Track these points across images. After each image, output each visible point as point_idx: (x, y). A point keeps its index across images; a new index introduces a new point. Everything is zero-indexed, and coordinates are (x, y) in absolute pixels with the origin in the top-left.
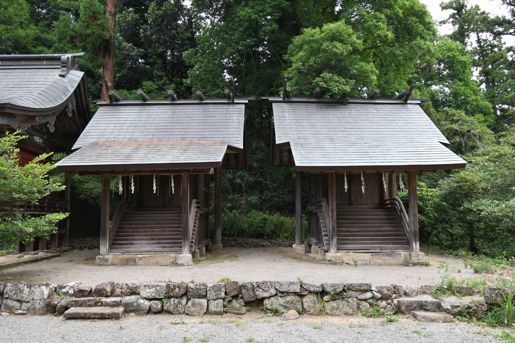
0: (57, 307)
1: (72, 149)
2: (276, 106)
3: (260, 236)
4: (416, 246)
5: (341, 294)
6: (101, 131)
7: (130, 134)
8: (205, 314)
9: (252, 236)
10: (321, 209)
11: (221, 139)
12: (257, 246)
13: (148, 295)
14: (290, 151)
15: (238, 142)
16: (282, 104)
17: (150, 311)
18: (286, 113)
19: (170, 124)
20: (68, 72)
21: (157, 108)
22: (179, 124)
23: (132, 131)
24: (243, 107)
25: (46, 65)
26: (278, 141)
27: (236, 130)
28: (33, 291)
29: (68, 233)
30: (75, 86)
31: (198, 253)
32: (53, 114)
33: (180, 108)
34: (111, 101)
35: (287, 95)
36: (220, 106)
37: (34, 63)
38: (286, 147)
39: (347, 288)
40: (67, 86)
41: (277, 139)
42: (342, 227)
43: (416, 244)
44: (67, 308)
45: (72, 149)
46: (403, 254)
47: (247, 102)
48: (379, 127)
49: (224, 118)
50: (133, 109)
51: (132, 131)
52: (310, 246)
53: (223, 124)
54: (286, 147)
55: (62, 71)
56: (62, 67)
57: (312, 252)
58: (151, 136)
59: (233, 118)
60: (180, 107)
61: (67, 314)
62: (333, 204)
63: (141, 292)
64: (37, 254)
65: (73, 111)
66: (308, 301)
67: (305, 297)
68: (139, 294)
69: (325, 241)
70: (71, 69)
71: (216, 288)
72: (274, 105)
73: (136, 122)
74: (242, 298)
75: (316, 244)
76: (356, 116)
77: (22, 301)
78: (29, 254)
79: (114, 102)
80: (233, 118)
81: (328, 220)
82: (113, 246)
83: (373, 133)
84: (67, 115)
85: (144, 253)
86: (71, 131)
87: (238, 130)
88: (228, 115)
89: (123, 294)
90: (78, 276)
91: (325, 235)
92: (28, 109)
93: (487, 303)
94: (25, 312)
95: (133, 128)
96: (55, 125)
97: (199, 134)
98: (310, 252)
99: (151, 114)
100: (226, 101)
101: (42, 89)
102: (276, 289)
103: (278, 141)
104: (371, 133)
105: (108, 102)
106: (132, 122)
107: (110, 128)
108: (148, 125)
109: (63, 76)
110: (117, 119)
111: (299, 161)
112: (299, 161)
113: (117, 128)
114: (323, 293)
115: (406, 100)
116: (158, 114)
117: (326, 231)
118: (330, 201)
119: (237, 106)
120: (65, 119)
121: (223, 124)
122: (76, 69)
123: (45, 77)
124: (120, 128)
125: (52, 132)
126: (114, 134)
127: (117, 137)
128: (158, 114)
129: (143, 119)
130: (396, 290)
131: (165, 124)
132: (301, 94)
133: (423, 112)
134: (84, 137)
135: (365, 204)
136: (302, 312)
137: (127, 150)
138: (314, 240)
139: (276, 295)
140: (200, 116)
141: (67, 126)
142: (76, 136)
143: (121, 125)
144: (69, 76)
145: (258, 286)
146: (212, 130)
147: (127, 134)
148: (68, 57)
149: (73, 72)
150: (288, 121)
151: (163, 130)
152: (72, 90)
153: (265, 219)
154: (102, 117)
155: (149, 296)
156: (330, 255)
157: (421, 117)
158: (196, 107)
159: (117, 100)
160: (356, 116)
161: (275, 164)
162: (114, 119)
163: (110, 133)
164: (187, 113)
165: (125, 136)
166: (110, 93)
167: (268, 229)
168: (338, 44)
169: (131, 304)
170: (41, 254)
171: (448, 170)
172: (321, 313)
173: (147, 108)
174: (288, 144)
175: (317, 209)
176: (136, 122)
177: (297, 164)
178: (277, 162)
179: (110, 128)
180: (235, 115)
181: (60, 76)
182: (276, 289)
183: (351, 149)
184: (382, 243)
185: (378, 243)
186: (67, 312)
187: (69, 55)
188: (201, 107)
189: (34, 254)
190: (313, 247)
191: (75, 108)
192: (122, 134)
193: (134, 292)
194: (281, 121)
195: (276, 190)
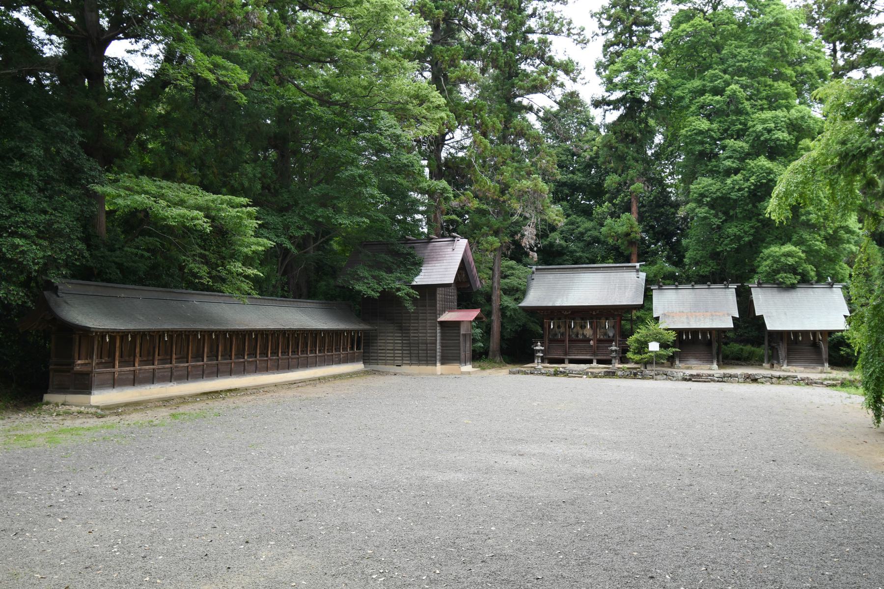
3: (738, 359)
4: (827, 365)
5: (785, 378)
9: (733, 359)
12: (737, 365)
17: (718, 381)
38: (761, 317)
39: (789, 376)
42: (262, 338)
43: (360, 279)
46: (820, 368)
54: (761, 317)
66: (774, 380)
71: (741, 375)
81: (782, 353)
82: (680, 361)
97: (715, 309)
111: (770, 327)
112: (770, 327)
114: (780, 377)
130: (808, 378)
132: (766, 283)
136: (772, 383)
153: (742, 349)
156: (783, 368)
167: (745, 355)
168: (790, 259)
172: (779, 384)
174: (762, 316)
195: (746, 328)
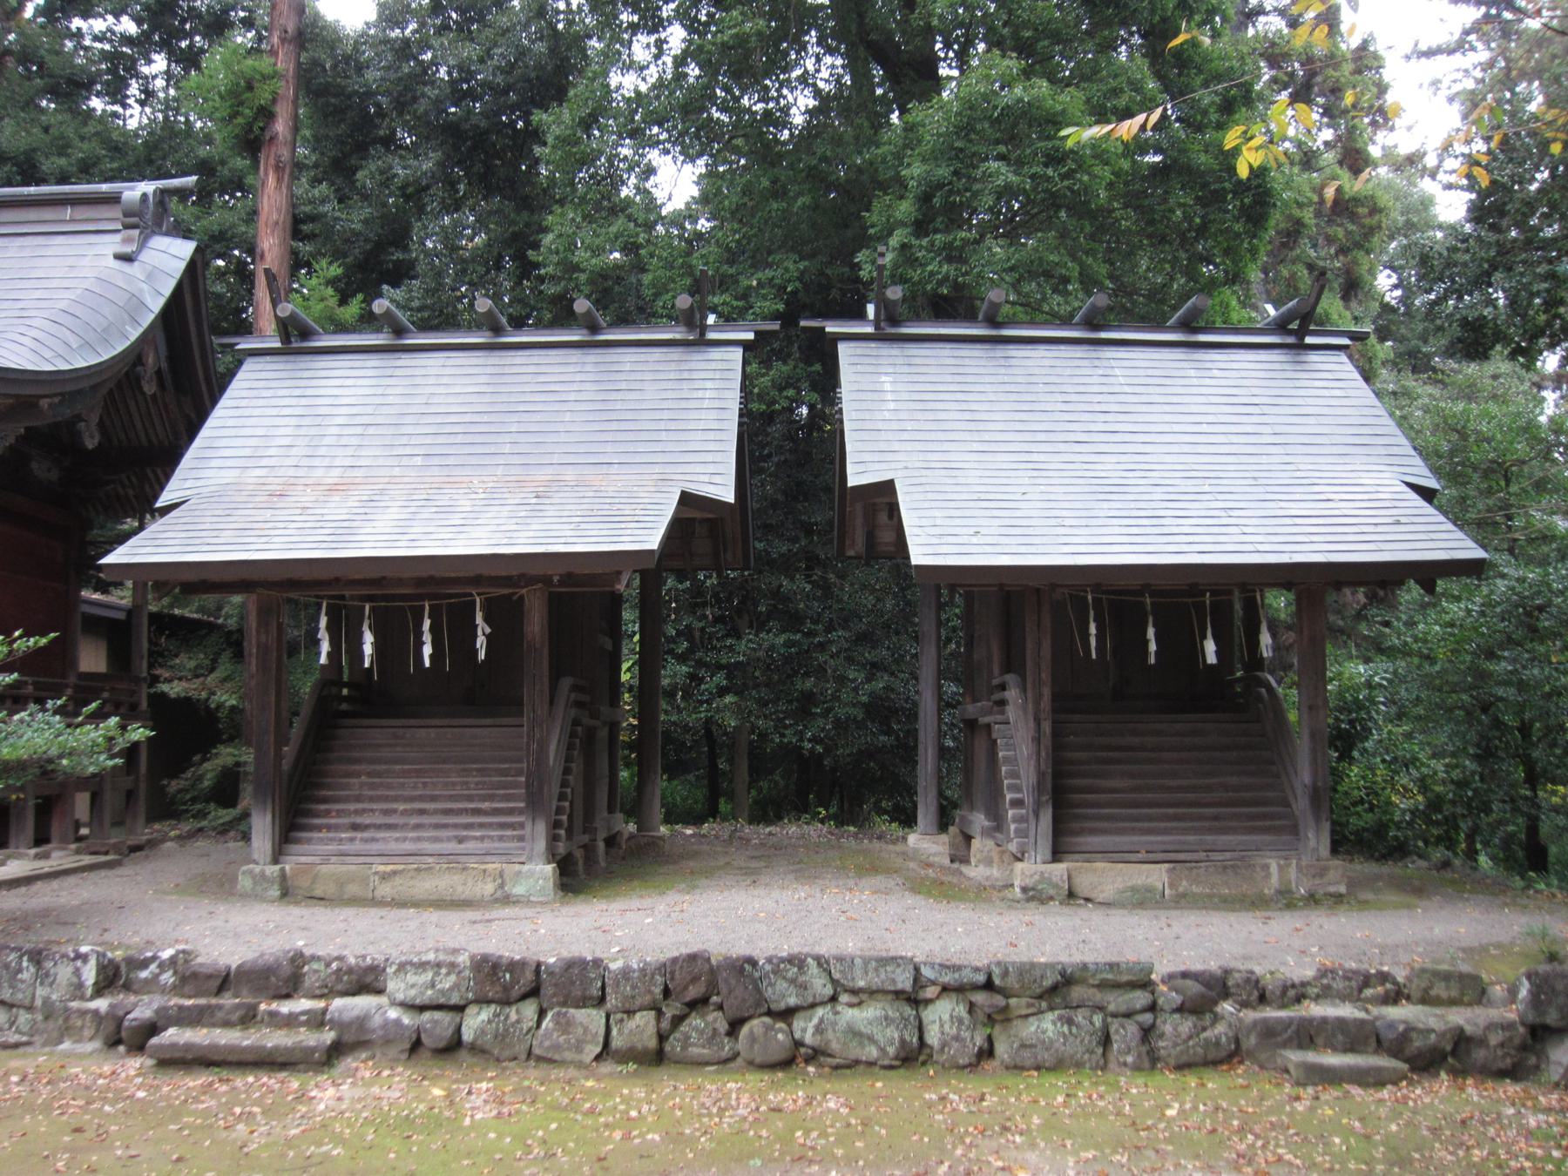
0: (126, 1023)
1: (158, 505)
2: (852, 352)
6: (253, 442)
7: (350, 451)
8: (598, 1058)
10: (1003, 713)
11: (657, 469)
13: (413, 992)
14: (894, 509)
15: (717, 479)
16: (873, 345)
18: (884, 378)
19: (485, 418)
20: (142, 245)
21: (441, 362)
22: (515, 418)
23: (354, 441)
24: (737, 354)
25: (72, 221)
26: (858, 474)
27: (711, 436)
28: (47, 975)
29: (143, 786)
30: (168, 288)
31: (581, 863)
32: (94, 388)
33: (518, 360)
34: (285, 336)
35: (891, 316)
36: (657, 354)
37: (32, 214)
40: (141, 290)
41: (850, 469)
44: (153, 1028)
45: (158, 505)
47: (750, 336)
48: (1204, 428)
49: (670, 395)
50: (358, 364)
51: (354, 441)
52: (968, 839)
53: (666, 415)
55: (127, 241)
56: (126, 227)
57: (973, 861)
58: (418, 461)
59: (700, 394)
60: (519, 357)
61: (161, 1047)
62: (1041, 695)
63: (391, 986)
64: (46, 856)
65: (159, 372)
67: (930, 1007)
68: (380, 992)
69: (1014, 821)
70: (154, 233)
72: (842, 348)
73: (369, 410)
74: (720, 1007)
75: (987, 833)
76: (1127, 389)
77: (12, 1006)
78: (19, 857)
79: (296, 338)
80: (700, 394)
83: (1186, 449)
84: (141, 388)
85: (396, 859)
86: (150, 441)
87: (719, 436)
88: (685, 385)
89: (328, 993)
90: (207, 916)
91: (1017, 803)
92: (20, 377)
93: (1523, 1024)
94: (24, 1039)
95: (359, 430)
96: (101, 425)
98: (965, 860)
99: (418, 381)
100: (678, 336)
101: (62, 305)
102: (834, 982)
103: (858, 474)
104: (1175, 449)
105: (276, 344)
106: (355, 410)
107: (282, 431)
108: (409, 420)
109: (127, 258)
110: (304, 401)
113: (303, 431)
115: (1302, 332)
116: (445, 380)
117: (1017, 789)
118: (1029, 686)
119: (716, 353)
120: (132, 404)
121: (666, 415)
122: (167, 234)
123: (70, 261)
124: (313, 431)
125: (90, 447)
126: (294, 451)
127: (305, 462)
128: (445, 380)
129: (390, 400)
131: (467, 418)
133: (1357, 376)
134: (194, 464)
135: (1159, 688)
137: (338, 508)
138: (979, 820)
139: (833, 999)
140: (588, 386)
141: (139, 426)
142: (168, 457)
143: (318, 420)
144: (146, 256)
145: (776, 972)
146: (631, 436)
147: (340, 452)
148: (145, 196)
149: (160, 242)
150: (892, 406)
151: (459, 439)
152: (156, 305)
154: (255, 393)
155: (414, 998)
157: (1351, 393)
158: (575, 355)
159: (306, 334)
160: (1127, 389)
161: (851, 553)
162: (294, 401)
163: (282, 452)
164: (542, 379)
165: (335, 462)
166: (283, 310)
169: (361, 1022)
170: (60, 858)
171: (1472, 568)
173: (406, 360)
174: (888, 487)
175: (991, 713)
176: (369, 410)
177: (921, 554)
178: (857, 546)
179: (282, 431)
180: (709, 385)
181: (120, 257)
182: (834, 982)
183: (1106, 505)
184: (1211, 831)
185: (1196, 831)
186: (154, 1041)
187: (148, 187)
188: (593, 357)
189: (37, 857)
190: (976, 844)
191: (164, 365)
192: (322, 451)
193: (366, 981)
194: (864, 406)
